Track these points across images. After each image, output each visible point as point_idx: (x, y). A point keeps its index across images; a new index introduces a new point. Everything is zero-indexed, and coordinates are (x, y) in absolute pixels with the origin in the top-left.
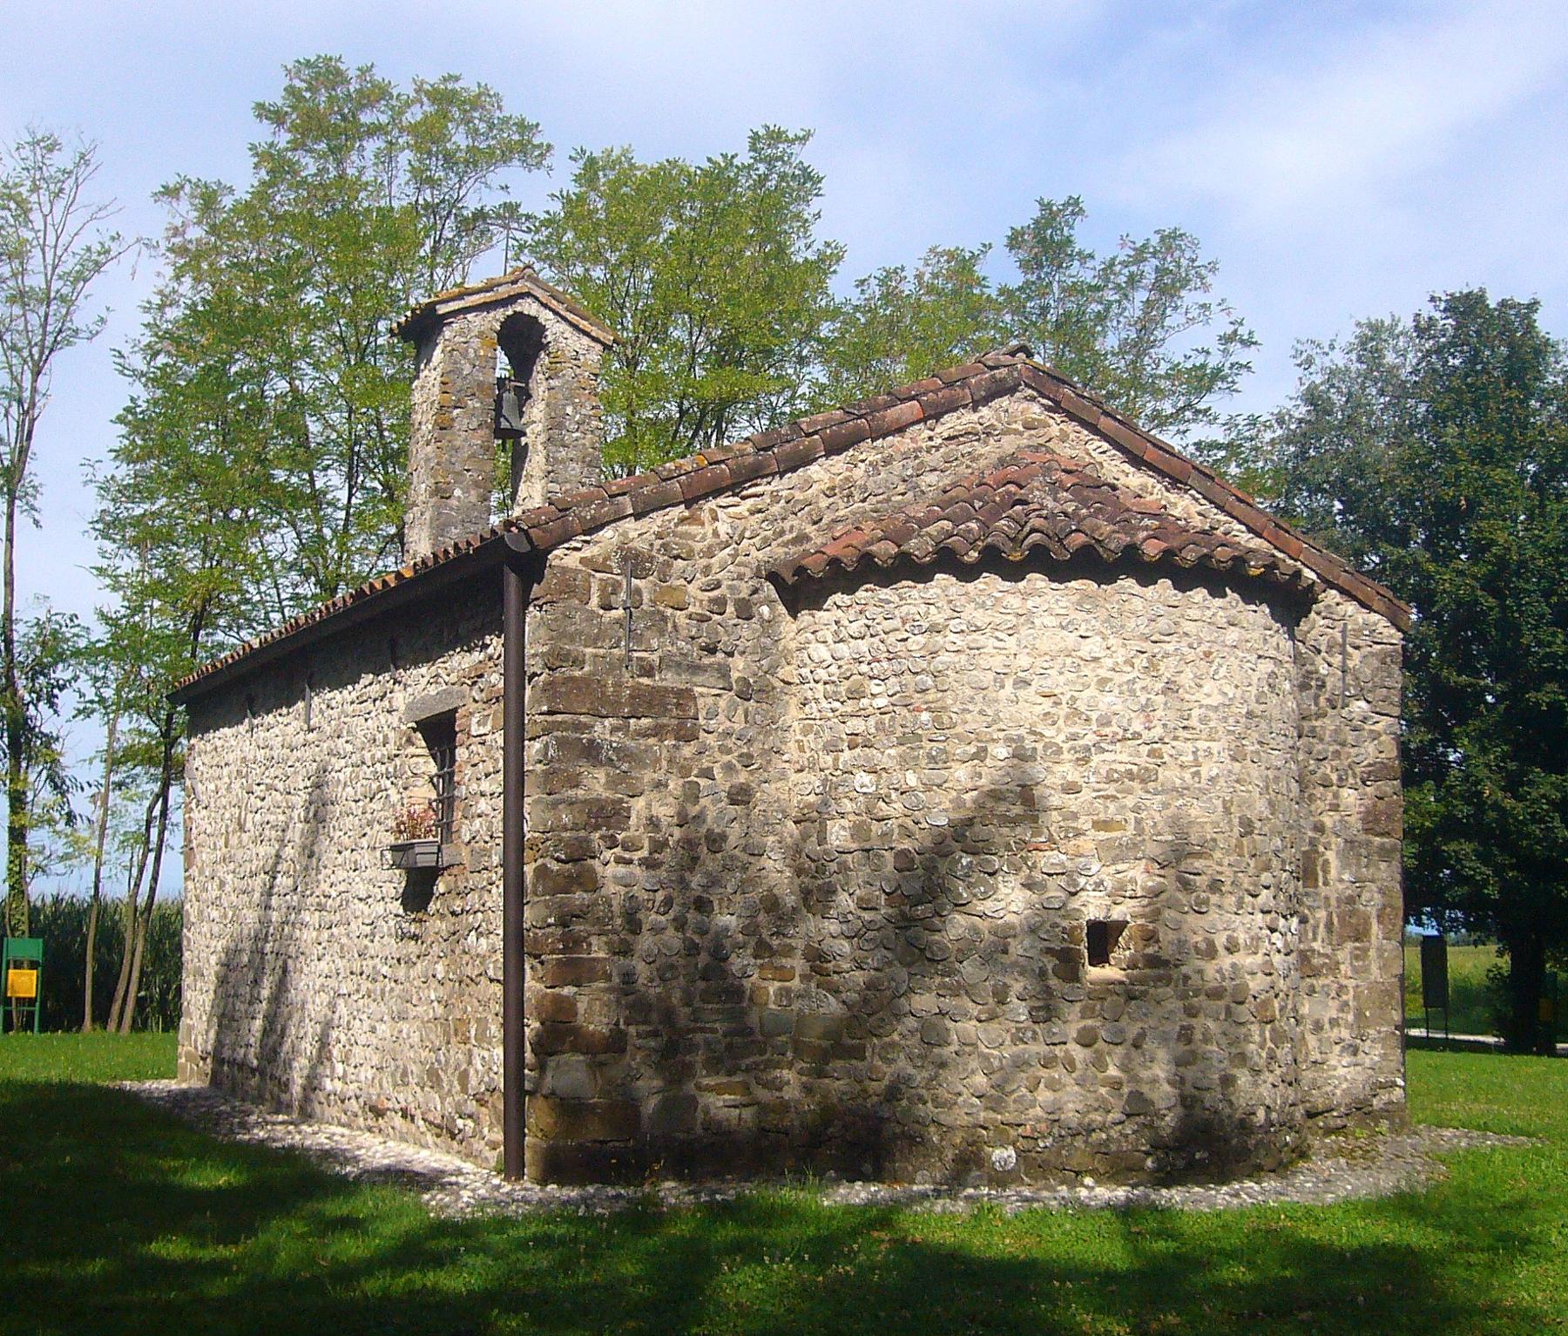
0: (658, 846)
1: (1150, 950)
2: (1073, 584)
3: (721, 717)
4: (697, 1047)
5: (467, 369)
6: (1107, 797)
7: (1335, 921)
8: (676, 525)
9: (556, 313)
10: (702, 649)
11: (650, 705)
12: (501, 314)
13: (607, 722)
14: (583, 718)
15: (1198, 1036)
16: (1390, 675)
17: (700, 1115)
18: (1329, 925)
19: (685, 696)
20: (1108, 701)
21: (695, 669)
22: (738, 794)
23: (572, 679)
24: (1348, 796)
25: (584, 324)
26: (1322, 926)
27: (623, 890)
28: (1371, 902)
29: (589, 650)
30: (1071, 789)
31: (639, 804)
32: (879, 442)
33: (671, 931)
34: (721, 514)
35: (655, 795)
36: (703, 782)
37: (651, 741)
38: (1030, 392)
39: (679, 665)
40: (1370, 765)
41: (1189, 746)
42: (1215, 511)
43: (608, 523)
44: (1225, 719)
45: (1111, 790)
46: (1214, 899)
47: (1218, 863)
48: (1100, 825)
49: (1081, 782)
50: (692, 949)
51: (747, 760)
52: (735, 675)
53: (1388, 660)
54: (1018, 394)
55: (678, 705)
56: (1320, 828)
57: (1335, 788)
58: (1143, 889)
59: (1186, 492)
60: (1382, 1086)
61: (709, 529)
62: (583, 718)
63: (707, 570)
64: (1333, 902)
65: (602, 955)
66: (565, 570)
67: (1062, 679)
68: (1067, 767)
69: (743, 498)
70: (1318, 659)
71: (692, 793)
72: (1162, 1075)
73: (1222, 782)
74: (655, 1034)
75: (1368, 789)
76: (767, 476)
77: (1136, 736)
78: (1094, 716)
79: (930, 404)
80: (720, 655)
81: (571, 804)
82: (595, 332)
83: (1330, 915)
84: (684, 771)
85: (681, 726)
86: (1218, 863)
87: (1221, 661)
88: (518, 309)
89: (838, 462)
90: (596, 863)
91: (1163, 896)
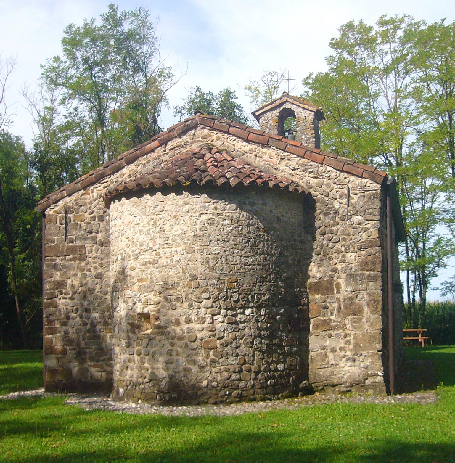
0: (74, 293)
1: (157, 323)
2: (132, 199)
3: (93, 252)
4: (87, 353)
5: (267, 131)
6: (141, 271)
7: (342, 307)
8: (81, 196)
9: (297, 105)
10: (88, 232)
11: (72, 251)
12: (278, 110)
13: (60, 258)
14: (53, 258)
15: (174, 353)
16: (373, 203)
17: (89, 373)
18: (339, 308)
19: (83, 247)
20: (143, 238)
21: (85, 239)
22: (98, 275)
23: (51, 246)
24: (351, 256)
25: (306, 107)
26: (335, 310)
27: (64, 307)
28: (363, 299)
29: (56, 237)
30: (133, 269)
31: (69, 281)
32: (145, 157)
33: (78, 318)
34: (95, 190)
35: (73, 278)
36: (88, 273)
37: (72, 262)
38: (202, 126)
39: (81, 238)
40: (363, 242)
41: (168, 250)
42: (282, 152)
43: (61, 199)
44: (183, 239)
45: (143, 268)
46: (178, 304)
47: (181, 291)
48: (140, 280)
49: (135, 266)
50: (85, 324)
51: (101, 265)
52: (98, 239)
53: (372, 197)
54: (198, 128)
55: (80, 251)
56: (335, 270)
57: (343, 253)
58: (153, 301)
59: (270, 147)
60: (371, 375)
61: (91, 195)
62: (53, 258)
63: (90, 208)
64: (341, 300)
65: (58, 326)
66: (49, 215)
67: (130, 232)
68: (132, 261)
69: (102, 184)
70: (335, 202)
71: (85, 277)
72: (161, 367)
73: (182, 262)
74: (74, 349)
75: (362, 252)
76: (108, 175)
77: (151, 248)
78: (138, 243)
79: (163, 139)
80: (94, 234)
81: (50, 282)
82: (310, 108)
83: (340, 305)
84: (82, 270)
85: (81, 257)
86: (181, 291)
87: (181, 218)
88: (284, 107)
89: (132, 166)
90: (57, 300)
91: (161, 304)
